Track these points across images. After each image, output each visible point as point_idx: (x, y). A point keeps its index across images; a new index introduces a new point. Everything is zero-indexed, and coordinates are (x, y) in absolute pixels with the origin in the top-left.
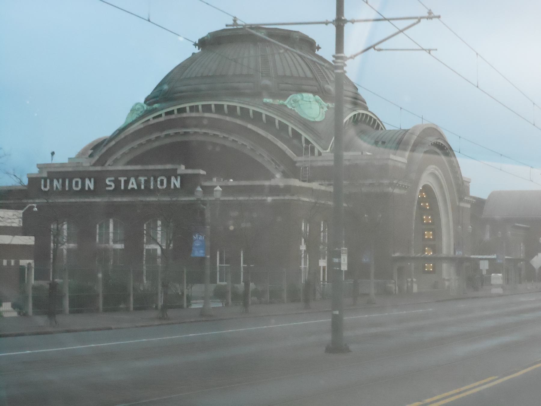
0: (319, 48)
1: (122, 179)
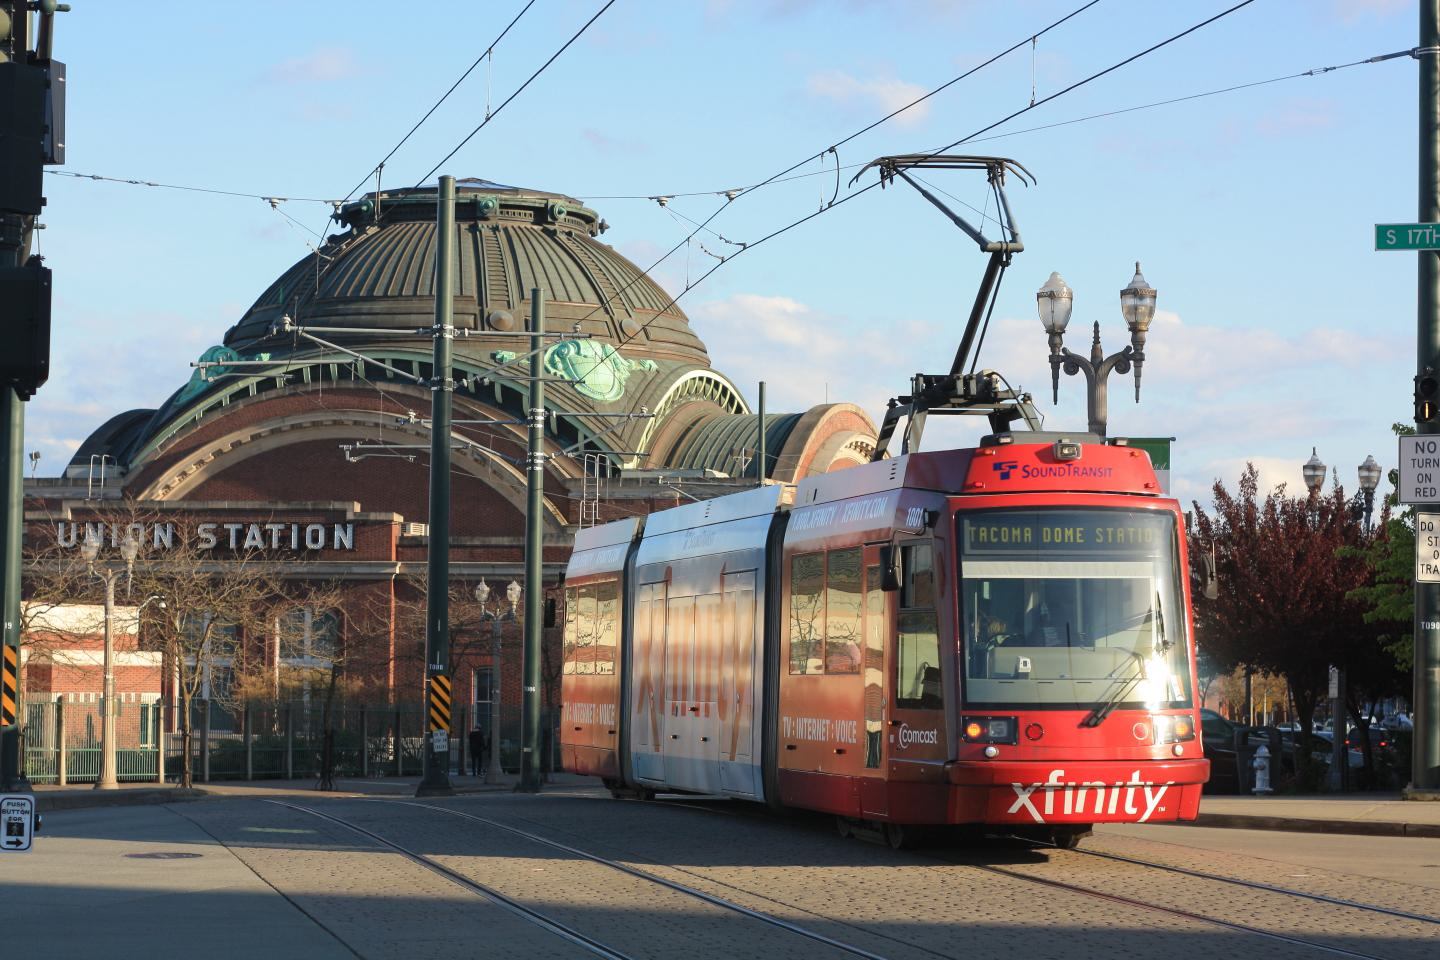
0: (603, 227)
1: (233, 528)
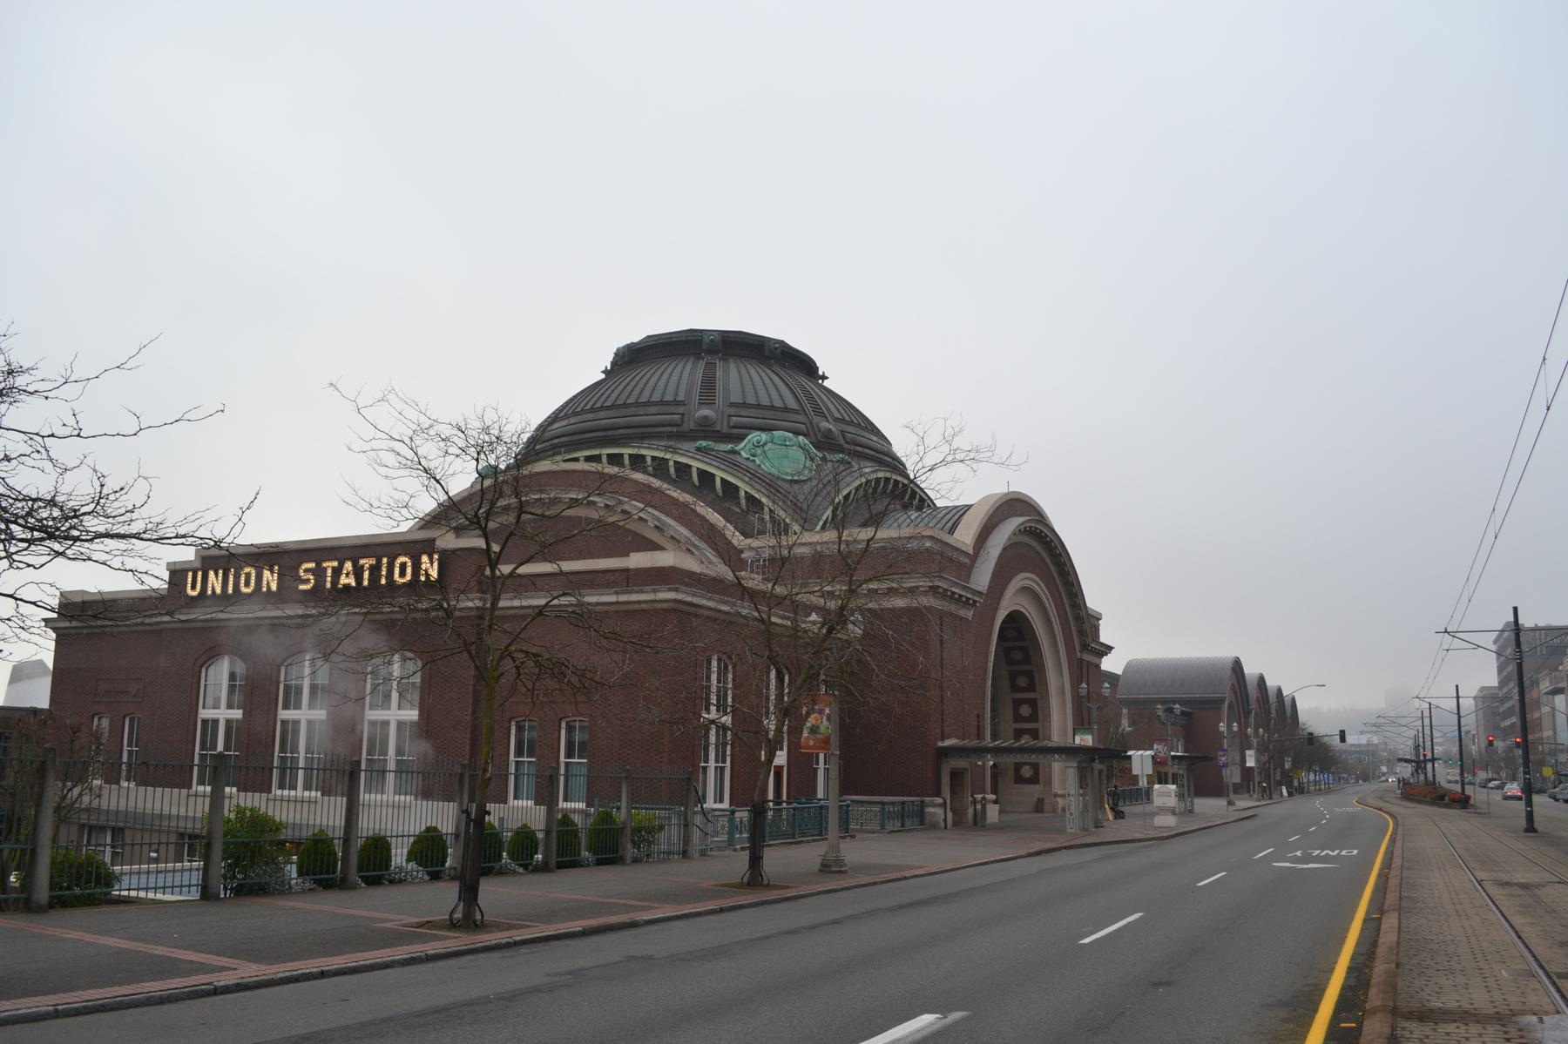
0: (824, 378)
